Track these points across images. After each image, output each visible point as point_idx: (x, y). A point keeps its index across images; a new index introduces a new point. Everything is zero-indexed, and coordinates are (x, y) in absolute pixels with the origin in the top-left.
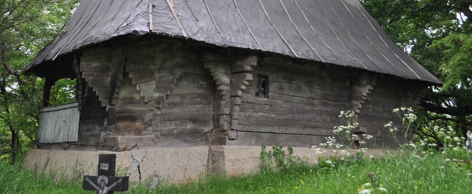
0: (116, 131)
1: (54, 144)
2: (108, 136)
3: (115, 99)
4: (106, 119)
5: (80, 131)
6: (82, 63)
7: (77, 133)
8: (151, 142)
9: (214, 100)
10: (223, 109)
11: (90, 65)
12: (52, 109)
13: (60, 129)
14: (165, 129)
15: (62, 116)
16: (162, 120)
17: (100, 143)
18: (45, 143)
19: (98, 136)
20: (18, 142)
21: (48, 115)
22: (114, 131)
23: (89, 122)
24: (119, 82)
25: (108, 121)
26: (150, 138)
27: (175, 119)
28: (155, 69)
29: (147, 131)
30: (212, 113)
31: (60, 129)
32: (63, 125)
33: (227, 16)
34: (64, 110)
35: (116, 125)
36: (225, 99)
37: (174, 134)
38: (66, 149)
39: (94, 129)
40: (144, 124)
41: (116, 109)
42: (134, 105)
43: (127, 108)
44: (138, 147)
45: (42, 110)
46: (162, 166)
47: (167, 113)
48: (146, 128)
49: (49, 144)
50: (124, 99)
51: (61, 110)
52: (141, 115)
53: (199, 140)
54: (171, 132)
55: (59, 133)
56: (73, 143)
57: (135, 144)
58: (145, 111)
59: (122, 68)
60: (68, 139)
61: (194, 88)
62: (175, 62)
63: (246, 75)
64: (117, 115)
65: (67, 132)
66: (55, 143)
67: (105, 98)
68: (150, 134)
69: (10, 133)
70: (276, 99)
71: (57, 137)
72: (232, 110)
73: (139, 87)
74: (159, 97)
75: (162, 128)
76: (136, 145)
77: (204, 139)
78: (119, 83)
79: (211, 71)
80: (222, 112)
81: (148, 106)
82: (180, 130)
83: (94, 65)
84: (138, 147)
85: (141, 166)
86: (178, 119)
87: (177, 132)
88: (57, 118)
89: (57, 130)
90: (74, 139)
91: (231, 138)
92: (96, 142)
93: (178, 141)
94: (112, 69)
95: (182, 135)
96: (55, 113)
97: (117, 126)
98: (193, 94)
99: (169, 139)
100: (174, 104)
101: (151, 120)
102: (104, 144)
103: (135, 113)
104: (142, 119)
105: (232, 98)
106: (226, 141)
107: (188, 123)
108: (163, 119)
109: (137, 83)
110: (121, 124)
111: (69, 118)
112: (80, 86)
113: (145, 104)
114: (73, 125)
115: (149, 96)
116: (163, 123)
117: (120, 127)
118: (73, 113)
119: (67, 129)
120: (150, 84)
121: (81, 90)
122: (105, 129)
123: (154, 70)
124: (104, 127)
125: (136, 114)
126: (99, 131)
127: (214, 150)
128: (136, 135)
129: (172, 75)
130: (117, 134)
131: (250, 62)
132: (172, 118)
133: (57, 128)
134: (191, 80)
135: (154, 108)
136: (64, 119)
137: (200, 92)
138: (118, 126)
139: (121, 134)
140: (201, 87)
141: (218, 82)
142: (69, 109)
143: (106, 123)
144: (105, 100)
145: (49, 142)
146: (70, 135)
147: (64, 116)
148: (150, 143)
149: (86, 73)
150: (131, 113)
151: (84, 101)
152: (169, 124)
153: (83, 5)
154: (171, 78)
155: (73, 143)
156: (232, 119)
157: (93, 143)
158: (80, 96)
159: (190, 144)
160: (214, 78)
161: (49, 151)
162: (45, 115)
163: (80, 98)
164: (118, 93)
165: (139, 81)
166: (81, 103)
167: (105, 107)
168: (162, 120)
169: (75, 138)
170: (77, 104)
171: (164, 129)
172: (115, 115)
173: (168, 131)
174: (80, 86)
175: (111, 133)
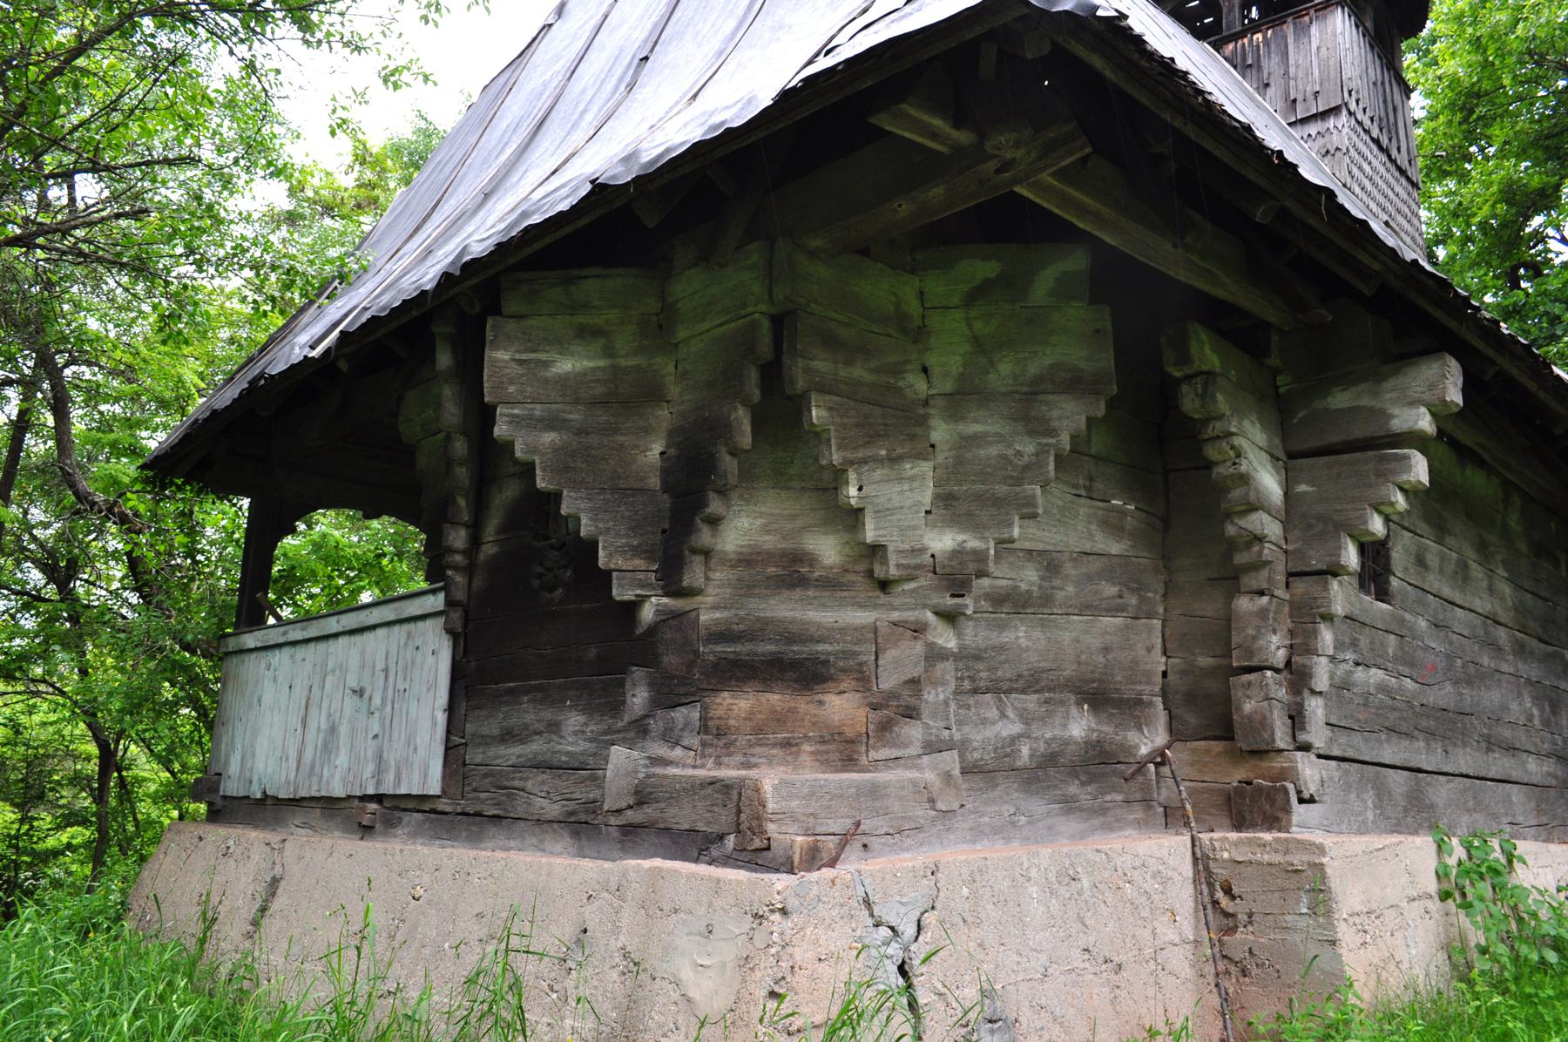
0: (704, 744)
1: (296, 802)
2: (658, 770)
3: (699, 559)
5: (456, 740)
6: (499, 357)
7: (439, 750)
8: (922, 813)
9: (1165, 596)
10: (1255, 638)
11: (546, 364)
12: (285, 633)
13: (333, 730)
14: (979, 737)
15: (343, 669)
16: (967, 685)
18: (248, 797)
19: (585, 769)
20: (122, 782)
21: (263, 665)
22: (694, 741)
24: (728, 458)
25: (651, 685)
26: (914, 783)
27: (1021, 684)
28: (929, 397)
29: (894, 746)
30: (1159, 662)
31: (333, 730)
32: (348, 711)
34: (357, 639)
35: (705, 709)
36: (1265, 586)
37: (1019, 764)
38: (366, 830)
39: (554, 727)
40: (875, 708)
41: (703, 618)
42: (810, 593)
43: (769, 614)
44: (865, 839)
45: (232, 644)
46: (1017, 959)
47: (986, 650)
48: (885, 727)
49: (269, 802)
50: (747, 560)
51: (336, 635)
52: (855, 654)
53: (1119, 797)
54: (1007, 756)
55: (328, 748)
56: (411, 805)
58: (876, 631)
59: (753, 375)
60: (378, 783)
61: (1093, 527)
62: (1048, 361)
63: (1407, 458)
64: (711, 652)
65: (372, 744)
66: (303, 799)
67: (636, 551)
68: (911, 762)
69: (92, 749)
70: (1410, 611)
71: (317, 770)
72: (1301, 644)
73: (860, 489)
74: (958, 553)
75: (966, 729)
77: (1138, 796)
78: (729, 464)
79: (1217, 427)
80: (1250, 653)
81: (896, 601)
82: (1042, 747)
83: (565, 366)
84: (865, 839)
85: (916, 965)
86: (1031, 683)
87: (1031, 756)
88: (316, 681)
89: (314, 738)
90: (416, 777)
91: (1306, 796)
92: (572, 806)
93: (1038, 806)
94: (674, 391)
95: (1052, 771)
96: (301, 652)
97: (712, 713)
98: (1091, 558)
99: (998, 791)
100: (1012, 603)
101: (914, 683)
102: (631, 816)
103: (818, 642)
104: (863, 679)
105: (1300, 586)
106: (1287, 810)
107: (1074, 711)
108: (973, 679)
109: (852, 463)
110: (737, 705)
111: (386, 677)
112: (462, 502)
113: (878, 593)
114: (413, 711)
115: (907, 547)
116: (971, 701)
117: (732, 722)
118: (411, 647)
119: (376, 729)
120: (912, 479)
121: (466, 525)
122: (639, 730)
123: (926, 403)
124: (626, 719)
125: (820, 647)
126: (591, 740)
127: (1226, 855)
128: (826, 764)
129: (1032, 433)
130: (710, 762)
131: (1432, 387)
132: (1008, 675)
133: (313, 723)
134: (1081, 482)
136: (352, 682)
137: (1115, 548)
138: (720, 712)
139: (739, 758)
140: (1112, 525)
141: (1236, 493)
142: (381, 632)
143: (638, 698)
144: (638, 563)
145: (269, 793)
146: (392, 758)
147: (354, 664)
148: (920, 813)
149: (516, 411)
150: (791, 638)
151: (477, 583)
152: (993, 713)
153: (439, 163)
154: (1028, 448)
155: (411, 805)
156: (1306, 693)
157: (554, 810)
158: (458, 558)
159: (1087, 820)
160: (1222, 470)
161: (274, 838)
162: (252, 666)
163: (456, 568)
164: (714, 522)
165: (860, 454)
166: (460, 595)
167: (633, 607)
168: (967, 685)
169: (426, 775)
170: (437, 602)
171: (978, 736)
172: (696, 652)
173: (996, 749)
174: (462, 502)
175: (678, 752)
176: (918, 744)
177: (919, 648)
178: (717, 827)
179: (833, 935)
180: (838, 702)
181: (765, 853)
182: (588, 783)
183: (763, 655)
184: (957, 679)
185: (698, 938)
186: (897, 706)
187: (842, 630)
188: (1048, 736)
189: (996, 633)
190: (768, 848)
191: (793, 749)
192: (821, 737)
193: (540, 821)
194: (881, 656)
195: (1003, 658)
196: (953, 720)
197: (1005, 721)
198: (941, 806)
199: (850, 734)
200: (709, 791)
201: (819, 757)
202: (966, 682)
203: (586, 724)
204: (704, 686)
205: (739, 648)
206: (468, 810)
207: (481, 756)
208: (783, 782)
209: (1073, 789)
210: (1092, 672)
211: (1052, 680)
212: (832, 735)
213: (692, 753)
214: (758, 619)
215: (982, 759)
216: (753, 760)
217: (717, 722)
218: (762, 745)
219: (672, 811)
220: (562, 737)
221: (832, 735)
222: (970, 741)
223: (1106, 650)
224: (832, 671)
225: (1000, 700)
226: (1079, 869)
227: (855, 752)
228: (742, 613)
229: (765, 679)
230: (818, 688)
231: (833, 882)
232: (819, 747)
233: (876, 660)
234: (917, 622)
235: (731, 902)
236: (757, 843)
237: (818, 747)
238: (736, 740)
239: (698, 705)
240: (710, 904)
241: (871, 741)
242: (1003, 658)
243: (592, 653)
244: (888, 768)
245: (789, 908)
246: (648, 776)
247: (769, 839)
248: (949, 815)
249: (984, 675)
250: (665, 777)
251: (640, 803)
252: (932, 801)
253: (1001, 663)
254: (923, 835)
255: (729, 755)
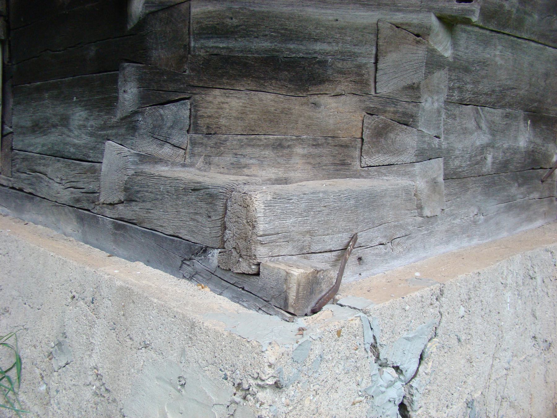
0: (194, 143)
2: (148, 168)
4: (130, 69)
14: (460, 146)
16: (456, 96)
17: (102, 200)
22: (184, 139)
23: (39, 90)
25: (141, 81)
26: (407, 191)
33: (80, 120)
39: (65, 121)
43: (264, 9)
52: (354, 55)
54: (477, 163)
57: (345, 238)
58: (377, 32)
75: (452, 138)
76: (354, 238)
92: (77, 194)
93: (492, 206)
102: (123, 211)
103: (316, 40)
107: (522, 124)
116: (457, 112)
117: (223, 121)
124: (119, 115)
125: (318, 47)
126: (91, 135)
130: (200, 162)
132: (486, 90)
135: (434, 21)
138: (210, 111)
139: (229, 158)
148: (410, 220)
152: (471, 124)
157: (66, 195)
172: (187, 47)
175: (167, 150)
176: (412, 151)
177: (421, 53)
178: (200, 238)
179: (336, 396)
180: (334, 105)
181: (253, 279)
182: (89, 174)
183: (257, 52)
184: (450, 89)
185: (170, 388)
186: (395, 113)
187: (342, 30)
188: (505, 146)
189: (481, 48)
190: (258, 274)
191: (286, 151)
192: (314, 140)
193: (58, 205)
194: (381, 59)
195: (483, 73)
196: (442, 130)
197: (479, 132)
198: (427, 212)
199: (345, 139)
200: (193, 197)
201: (312, 161)
202: (456, 93)
203: (87, 119)
204: (195, 83)
205: (232, 44)
206: (15, 185)
207: (21, 143)
208: (277, 197)
209: (514, 190)
210: (536, 93)
211: (513, 98)
212: (326, 138)
213: (182, 152)
214: (253, 14)
215: (460, 167)
216: (243, 161)
217: (208, 121)
218: (253, 146)
219: (157, 213)
220: (70, 131)
221: (326, 138)
222: (453, 149)
223: (547, 75)
224: (330, 72)
225: (477, 112)
226: (536, 270)
227: (348, 156)
228: (236, 6)
229: (259, 78)
230: (313, 89)
231: (339, 333)
232: (312, 150)
233: (376, 63)
234: (421, 26)
235: (208, 357)
236: (244, 267)
237: (311, 150)
238: (226, 140)
239: (188, 102)
240: (183, 352)
241: (365, 147)
242: (483, 73)
243: (92, 51)
244: (380, 174)
245: (283, 382)
246: (137, 174)
247: (258, 264)
248: (432, 220)
249: (469, 87)
250: (152, 176)
251: (129, 200)
252: (420, 207)
253: (483, 77)
254: (411, 241)
255: (220, 154)
